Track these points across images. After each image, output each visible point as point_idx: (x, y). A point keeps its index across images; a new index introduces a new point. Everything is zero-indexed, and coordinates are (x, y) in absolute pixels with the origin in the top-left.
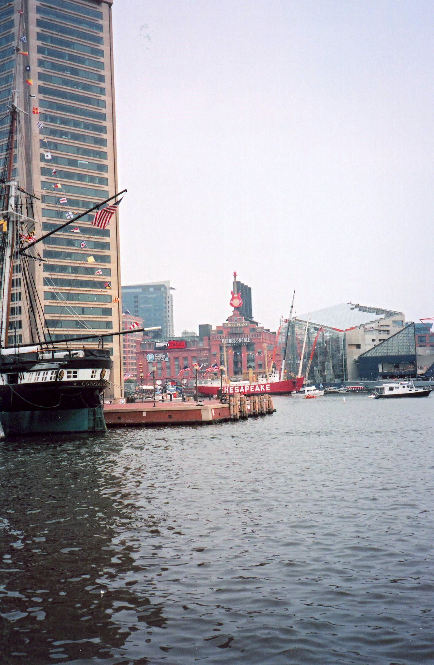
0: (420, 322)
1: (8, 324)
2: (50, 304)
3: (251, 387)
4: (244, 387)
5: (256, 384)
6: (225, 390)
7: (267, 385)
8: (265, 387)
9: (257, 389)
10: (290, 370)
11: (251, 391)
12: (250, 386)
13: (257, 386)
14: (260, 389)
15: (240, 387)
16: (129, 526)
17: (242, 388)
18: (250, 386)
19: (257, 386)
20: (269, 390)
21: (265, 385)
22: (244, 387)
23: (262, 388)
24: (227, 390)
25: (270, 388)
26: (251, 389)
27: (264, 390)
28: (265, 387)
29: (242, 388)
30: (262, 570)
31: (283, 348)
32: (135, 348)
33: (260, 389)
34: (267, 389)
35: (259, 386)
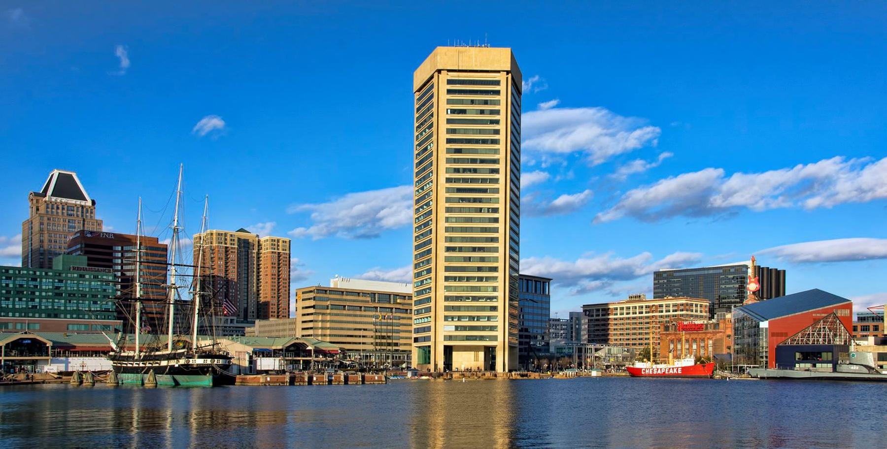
0: (867, 311)
1: (7, 269)
2: (418, 290)
3: (667, 369)
4: (661, 369)
5: (671, 366)
6: (647, 371)
7: (679, 369)
8: (677, 370)
9: (671, 371)
10: (739, 278)
11: (666, 373)
12: (665, 369)
13: (671, 369)
14: (673, 371)
15: (658, 369)
16: (653, 403)
17: (659, 370)
18: (665, 369)
19: (671, 369)
20: (681, 373)
21: (678, 368)
22: (661, 369)
23: (675, 371)
24: (648, 371)
25: (682, 371)
26: (667, 371)
27: (676, 372)
28: (677, 370)
29: (659, 370)
30: (697, 272)
31: (219, 350)
32: (845, 344)
33: (673, 371)
34: (679, 372)
35: (673, 368)
